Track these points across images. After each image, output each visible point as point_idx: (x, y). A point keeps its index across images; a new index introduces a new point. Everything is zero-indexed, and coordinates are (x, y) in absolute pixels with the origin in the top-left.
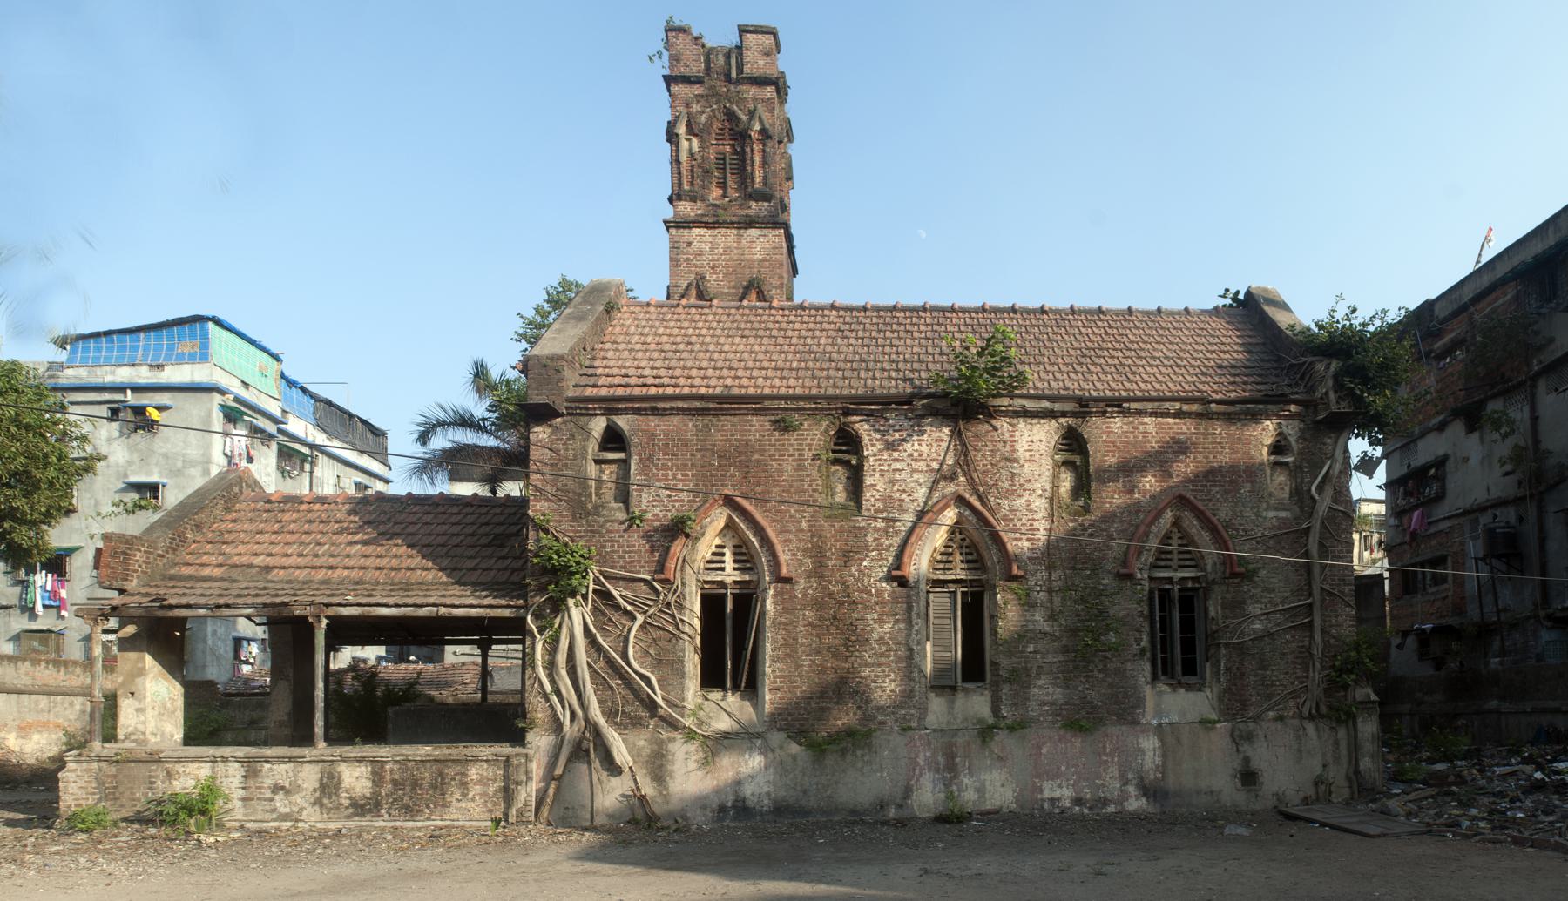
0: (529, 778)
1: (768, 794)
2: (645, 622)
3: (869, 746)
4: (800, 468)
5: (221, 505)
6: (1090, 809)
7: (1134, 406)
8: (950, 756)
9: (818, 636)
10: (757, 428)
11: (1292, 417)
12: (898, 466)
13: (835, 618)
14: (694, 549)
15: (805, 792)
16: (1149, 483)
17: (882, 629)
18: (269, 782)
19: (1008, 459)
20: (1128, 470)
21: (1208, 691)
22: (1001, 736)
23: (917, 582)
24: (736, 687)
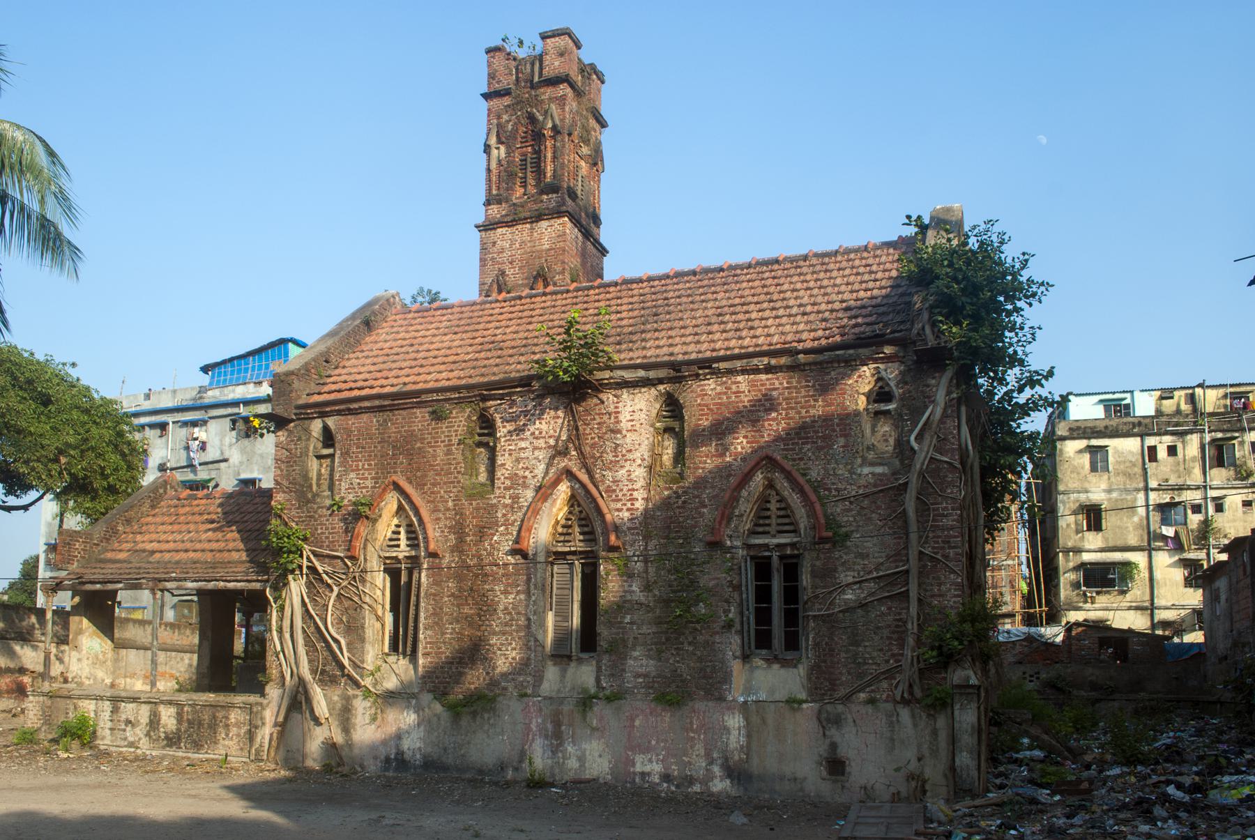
0: (263, 724)
1: (420, 749)
2: (339, 595)
3: (493, 710)
4: (449, 453)
5: (147, 503)
6: (677, 786)
7: (723, 365)
8: (557, 724)
9: (458, 606)
10: (420, 416)
11: (889, 359)
12: (523, 444)
13: (471, 589)
14: (374, 530)
15: (445, 749)
16: (741, 443)
17: (506, 599)
18: (124, 717)
19: (613, 431)
20: (720, 431)
21: (801, 667)
22: (599, 708)
23: (535, 555)
24: (405, 655)
